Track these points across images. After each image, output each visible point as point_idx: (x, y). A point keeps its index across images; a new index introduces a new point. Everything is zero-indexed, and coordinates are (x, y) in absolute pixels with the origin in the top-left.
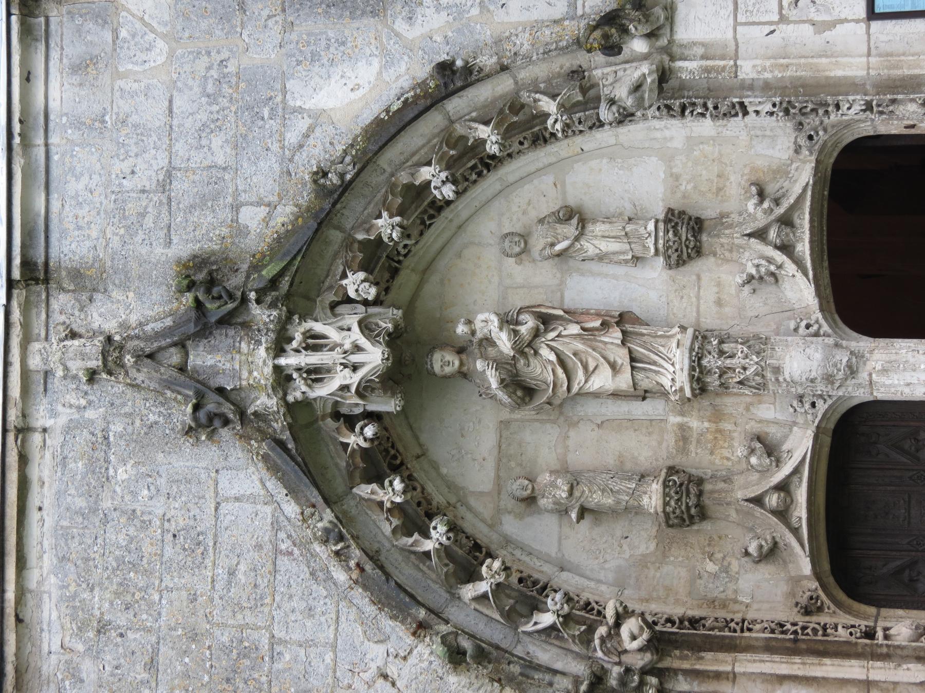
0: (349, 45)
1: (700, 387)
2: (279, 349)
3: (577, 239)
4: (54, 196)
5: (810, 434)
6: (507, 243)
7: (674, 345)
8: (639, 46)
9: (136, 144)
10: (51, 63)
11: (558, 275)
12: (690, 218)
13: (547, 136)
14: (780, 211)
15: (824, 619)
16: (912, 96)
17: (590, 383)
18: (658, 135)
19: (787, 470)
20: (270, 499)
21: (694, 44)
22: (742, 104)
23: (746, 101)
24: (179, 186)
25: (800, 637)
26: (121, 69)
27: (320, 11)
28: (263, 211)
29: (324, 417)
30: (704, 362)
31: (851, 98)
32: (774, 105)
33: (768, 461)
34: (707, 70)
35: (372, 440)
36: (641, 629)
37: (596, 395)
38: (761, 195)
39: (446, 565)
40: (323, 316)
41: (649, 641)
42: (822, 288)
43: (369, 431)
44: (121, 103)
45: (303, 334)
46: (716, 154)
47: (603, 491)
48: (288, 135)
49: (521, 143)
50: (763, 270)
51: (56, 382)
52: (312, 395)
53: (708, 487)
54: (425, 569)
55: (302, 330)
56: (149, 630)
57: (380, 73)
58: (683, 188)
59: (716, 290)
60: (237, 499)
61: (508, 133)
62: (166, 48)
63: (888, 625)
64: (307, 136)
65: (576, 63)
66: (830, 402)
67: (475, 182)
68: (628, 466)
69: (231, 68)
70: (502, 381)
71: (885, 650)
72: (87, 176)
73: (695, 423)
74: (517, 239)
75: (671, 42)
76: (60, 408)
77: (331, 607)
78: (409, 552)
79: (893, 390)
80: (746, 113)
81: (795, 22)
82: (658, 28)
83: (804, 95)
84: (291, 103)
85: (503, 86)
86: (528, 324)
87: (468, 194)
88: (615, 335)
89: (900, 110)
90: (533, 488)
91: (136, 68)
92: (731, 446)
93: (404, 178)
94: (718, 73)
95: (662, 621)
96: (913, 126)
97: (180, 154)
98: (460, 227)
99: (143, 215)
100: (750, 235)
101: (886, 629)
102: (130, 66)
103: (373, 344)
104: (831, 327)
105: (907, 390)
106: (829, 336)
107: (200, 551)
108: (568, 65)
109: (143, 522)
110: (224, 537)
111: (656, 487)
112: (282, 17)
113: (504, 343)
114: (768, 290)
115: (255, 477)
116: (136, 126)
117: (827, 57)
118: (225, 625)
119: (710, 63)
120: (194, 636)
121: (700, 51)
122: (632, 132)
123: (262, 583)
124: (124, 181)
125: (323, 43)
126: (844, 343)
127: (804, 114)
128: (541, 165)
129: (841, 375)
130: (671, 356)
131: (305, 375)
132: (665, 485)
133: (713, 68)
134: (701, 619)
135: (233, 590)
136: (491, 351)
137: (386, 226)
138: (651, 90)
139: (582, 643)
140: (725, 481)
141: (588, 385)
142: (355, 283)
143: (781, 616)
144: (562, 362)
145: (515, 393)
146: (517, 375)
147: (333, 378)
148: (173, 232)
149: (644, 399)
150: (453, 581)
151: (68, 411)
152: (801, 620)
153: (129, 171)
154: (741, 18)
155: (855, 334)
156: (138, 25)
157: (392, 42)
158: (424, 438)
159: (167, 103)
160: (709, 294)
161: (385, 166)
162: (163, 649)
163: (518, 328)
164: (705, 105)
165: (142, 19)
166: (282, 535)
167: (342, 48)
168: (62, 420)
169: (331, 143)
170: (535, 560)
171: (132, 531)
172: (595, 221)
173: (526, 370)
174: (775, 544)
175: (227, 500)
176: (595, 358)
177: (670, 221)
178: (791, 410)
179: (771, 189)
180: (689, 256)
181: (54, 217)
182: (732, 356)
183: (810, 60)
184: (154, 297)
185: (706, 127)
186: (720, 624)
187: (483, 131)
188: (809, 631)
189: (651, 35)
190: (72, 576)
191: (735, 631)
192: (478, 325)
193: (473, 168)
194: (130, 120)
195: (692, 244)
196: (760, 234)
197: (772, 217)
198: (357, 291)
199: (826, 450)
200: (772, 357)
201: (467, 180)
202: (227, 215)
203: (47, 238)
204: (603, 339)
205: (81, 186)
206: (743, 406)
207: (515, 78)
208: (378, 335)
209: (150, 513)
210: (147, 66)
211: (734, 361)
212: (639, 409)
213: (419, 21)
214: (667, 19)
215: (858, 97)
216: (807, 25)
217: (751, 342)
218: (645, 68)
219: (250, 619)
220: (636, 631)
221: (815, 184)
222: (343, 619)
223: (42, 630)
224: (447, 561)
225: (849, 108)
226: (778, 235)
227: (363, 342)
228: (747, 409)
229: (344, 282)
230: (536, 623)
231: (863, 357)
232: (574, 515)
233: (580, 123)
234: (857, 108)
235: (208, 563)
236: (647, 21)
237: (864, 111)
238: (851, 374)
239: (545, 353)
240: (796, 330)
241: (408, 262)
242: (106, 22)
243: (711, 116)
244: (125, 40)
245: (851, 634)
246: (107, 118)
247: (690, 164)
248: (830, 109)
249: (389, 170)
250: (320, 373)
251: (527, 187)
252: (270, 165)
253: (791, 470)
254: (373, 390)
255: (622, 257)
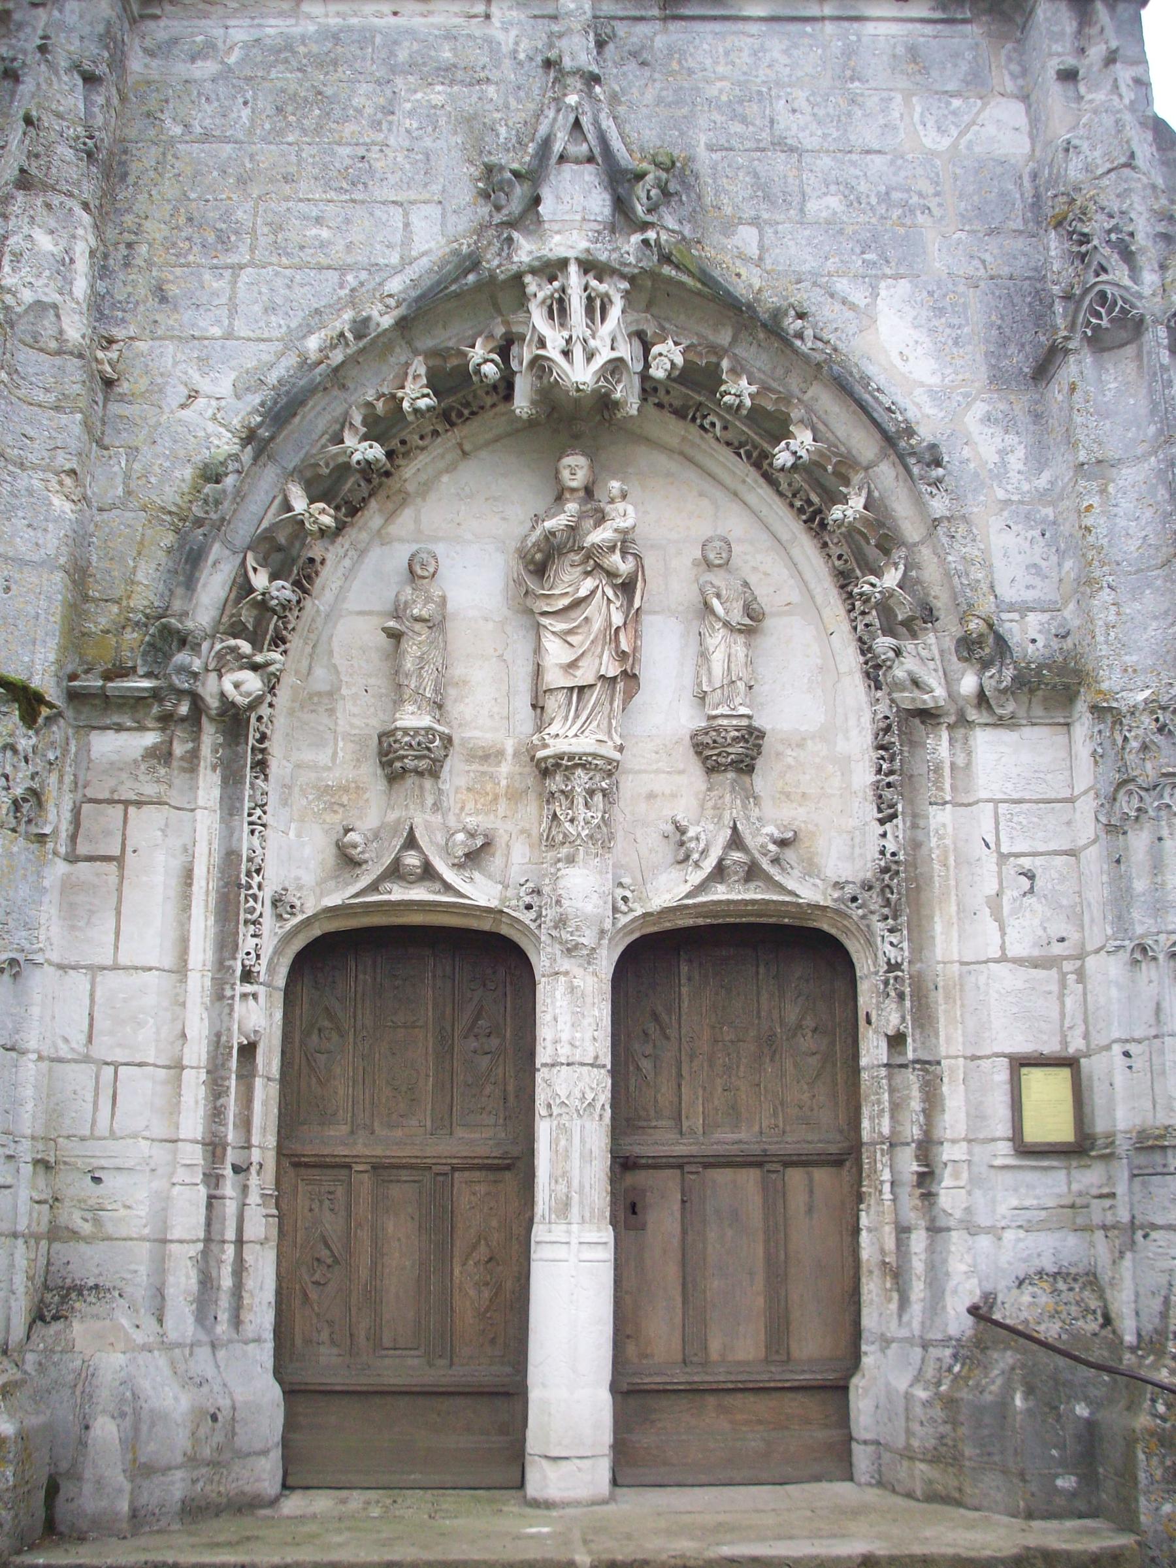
0: (955, 350)
1: (546, 769)
2: (588, 266)
3: (726, 624)
4: (764, 27)
5: (494, 904)
6: (718, 544)
7: (600, 737)
8: (968, 684)
9: (828, 115)
10: (918, 26)
11: (681, 608)
12: (753, 759)
13: (849, 588)
14: (765, 864)
15: (268, 921)
16: (908, 1017)
17: (552, 637)
18: (852, 722)
19: (450, 876)
20: (407, 262)
21: (969, 754)
22: (894, 816)
23: (899, 821)
24: (780, 163)
25: (243, 892)
26: (914, 99)
27: (993, 318)
28: (754, 252)
29: (506, 323)
30: (579, 772)
31: (905, 945)
32: (893, 854)
33: (460, 853)
34: (938, 769)
35: (478, 371)
36: (249, 694)
37: (538, 649)
38: (783, 843)
39: (327, 465)
40: (630, 318)
41: (233, 704)
42: (671, 916)
43: (489, 369)
44: (876, 99)
45: (607, 295)
46: (829, 791)
47: (421, 658)
48: (845, 281)
49: (840, 557)
50: (693, 845)
51: (544, 26)
52: (533, 306)
53: (428, 783)
54: (323, 441)
55: (611, 292)
56: (250, 132)
57: (922, 384)
58: (789, 752)
59: (664, 785)
60: (407, 225)
61: (852, 534)
62: (941, 148)
63: (262, 998)
64: (844, 302)
65: (942, 614)
66: (533, 926)
67: (792, 505)
68: (452, 692)
69: (921, 219)
70: (553, 534)
71: (228, 993)
72: (788, 61)
73: (505, 769)
74: (724, 555)
75: (970, 724)
76: (514, 32)
77: (276, 334)
78: (344, 421)
79: (549, 1001)
80: (882, 822)
81: (1000, 873)
82: (989, 707)
83: (908, 889)
84: (883, 284)
85: (911, 530)
86: (624, 567)
87: (776, 498)
88: (612, 669)
89: (891, 1005)
90: (424, 578)
91: (917, 117)
92: (477, 812)
93: (796, 413)
94: (935, 783)
95: (263, 728)
96: (869, 1022)
97: (818, 162)
98: (736, 494)
99: (744, 121)
100: (735, 828)
101: (255, 996)
102: (918, 109)
103: (596, 372)
104: (625, 926)
105: (548, 1017)
106: (614, 924)
107: (345, 185)
108: (939, 605)
109: (380, 123)
110: (360, 211)
111: (426, 721)
112: (985, 275)
113: (599, 536)
114: (665, 852)
115: (433, 244)
116: (849, 115)
117: (958, 913)
118: (256, 215)
119: (947, 772)
120: (243, 182)
121: (961, 761)
122: (855, 687)
123: (307, 255)
124: (783, 102)
125: (956, 321)
126: (605, 942)
127: (882, 890)
128: (812, 586)
129: (565, 936)
130: (587, 733)
131: (556, 295)
132: (428, 730)
133: (942, 776)
134: (266, 776)
135: (297, 222)
136: (588, 523)
137: (740, 390)
138: (913, 699)
139: (233, 625)
140: (435, 804)
141: (549, 635)
142: (668, 355)
143: (270, 870)
144: (577, 604)
145: (539, 550)
146: (560, 554)
147: (554, 328)
148: (724, 153)
149: (534, 706)
150: (308, 474)
151: (511, 41)
152: (267, 894)
153: (796, 106)
154: (1002, 807)
155: (616, 957)
156: (966, 119)
157: (960, 398)
158: (483, 454)
159: (877, 148)
160: (661, 784)
161: (810, 394)
162: (229, 148)
163: (618, 552)
164: (891, 772)
165: (974, 123)
166: (364, 275)
167: (950, 342)
168: (500, 36)
169: (836, 329)
170: (339, 583)
171: (368, 111)
172: (748, 645)
173: (567, 563)
174: (358, 864)
175: (406, 214)
176: (582, 643)
177: (751, 734)
178: (522, 881)
179: (789, 855)
180: (708, 758)
181: (740, 26)
182: (587, 805)
183: (953, 892)
184: (647, 131)
185: (864, 776)
186: (259, 797)
187: (857, 503)
188: (251, 903)
189: (982, 699)
190: (315, 49)
191: (250, 815)
192: (620, 506)
193: (809, 502)
194: (856, 108)
195: (721, 760)
196: (736, 841)
197: (757, 855)
198: (660, 354)
199: (474, 924)
200: (587, 853)
201: (794, 496)
202: (748, 213)
203: (715, 18)
204: (606, 653)
205: (776, 54)
206: (527, 826)
207: (922, 542)
208: (606, 380)
209: (390, 130)
210: (920, 127)
211: (581, 807)
212: (523, 702)
213: (986, 430)
214: (1001, 718)
215: (906, 954)
216: (996, 887)
217: (604, 829)
218: (940, 692)
219: (262, 241)
220: (244, 688)
221: (799, 905)
222: (262, 346)
223: (253, 18)
224: (332, 465)
225: (891, 944)
226: (735, 862)
227: (599, 362)
228: (522, 831)
229: (670, 342)
230: (255, 570)
231: (589, 963)
232: (391, 624)
233: (867, 625)
234: (892, 954)
235: (332, 195)
236: (1000, 691)
237: (889, 963)
238: (568, 950)
239: (588, 585)
240: (620, 885)
241: (694, 430)
242: (968, 83)
243: (878, 781)
244: (948, 104)
245: (248, 954)
246: (857, 84)
247: (817, 760)
248: (890, 921)
249: (806, 398)
250: (559, 317)
251: (786, 572)
252: (808, 262)
253: (449, 880)
254: (540, 378)
255: (704, 679)
